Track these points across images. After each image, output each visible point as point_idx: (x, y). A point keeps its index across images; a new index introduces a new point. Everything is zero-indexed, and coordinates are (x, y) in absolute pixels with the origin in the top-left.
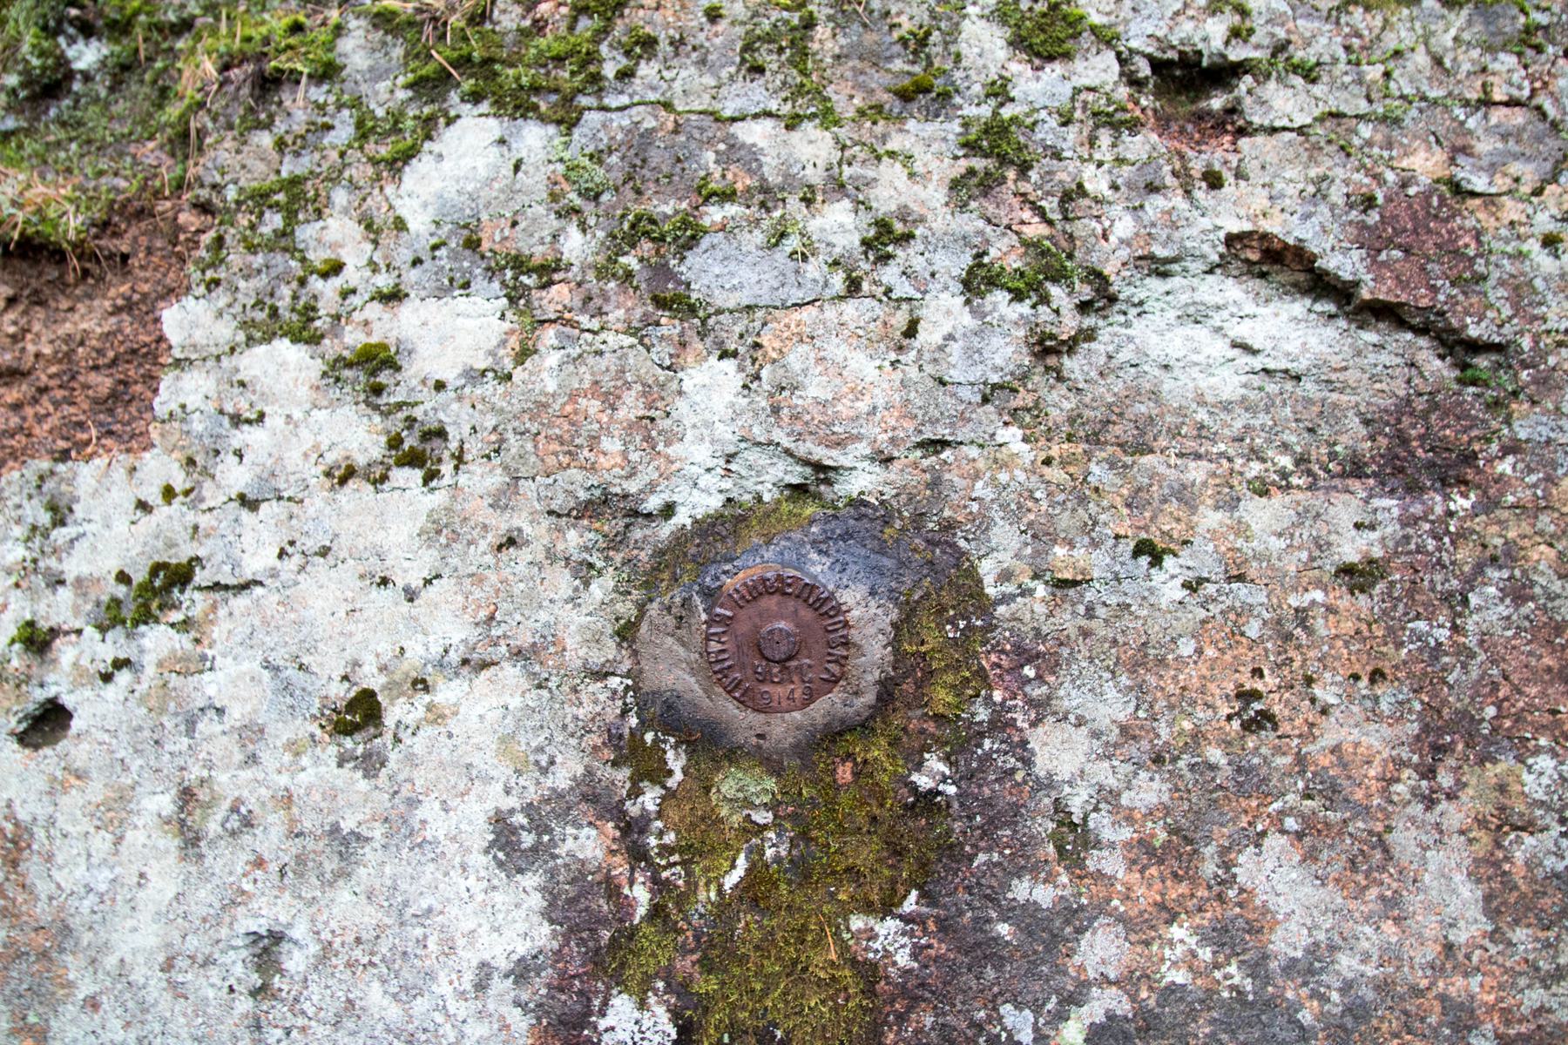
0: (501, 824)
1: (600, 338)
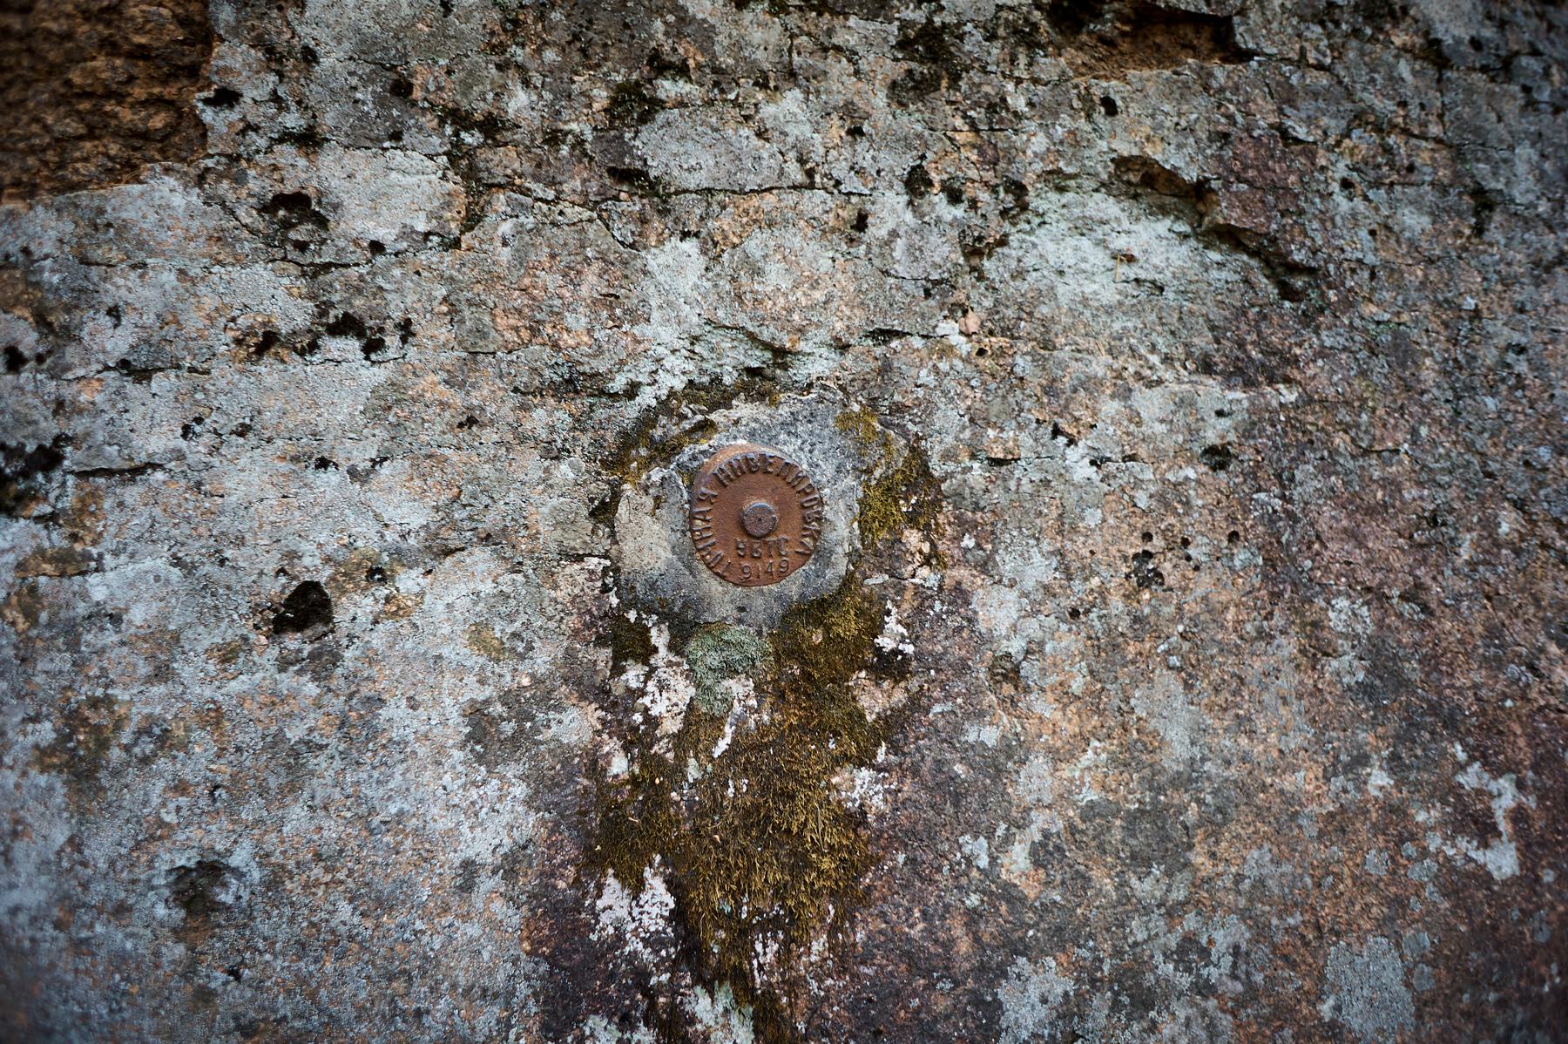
0: (477, 715)
1: (556, 209)
